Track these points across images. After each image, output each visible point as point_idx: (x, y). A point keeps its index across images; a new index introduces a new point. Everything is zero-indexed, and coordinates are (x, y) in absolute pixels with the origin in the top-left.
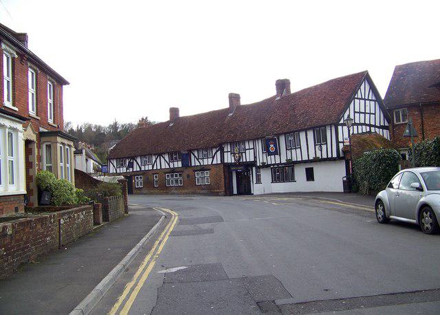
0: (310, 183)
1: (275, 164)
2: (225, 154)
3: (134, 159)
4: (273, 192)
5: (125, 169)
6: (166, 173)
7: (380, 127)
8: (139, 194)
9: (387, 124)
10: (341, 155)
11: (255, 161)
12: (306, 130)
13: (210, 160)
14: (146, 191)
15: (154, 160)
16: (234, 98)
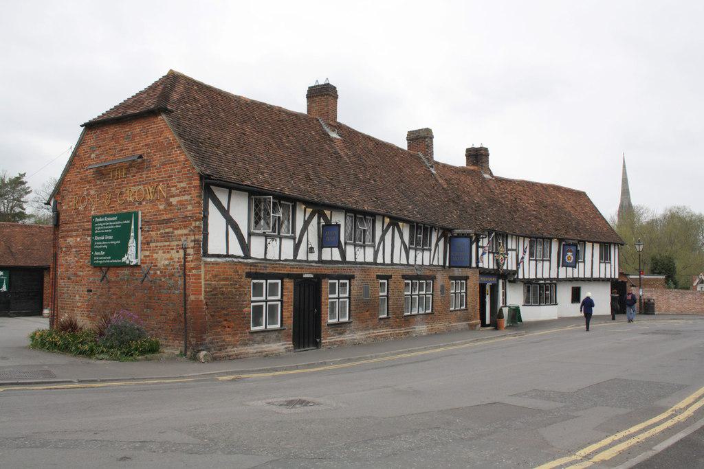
1: (550, 279)
11: (516, 272)
13: (370, 252)
14: (359, 336)
15: (299, 224)
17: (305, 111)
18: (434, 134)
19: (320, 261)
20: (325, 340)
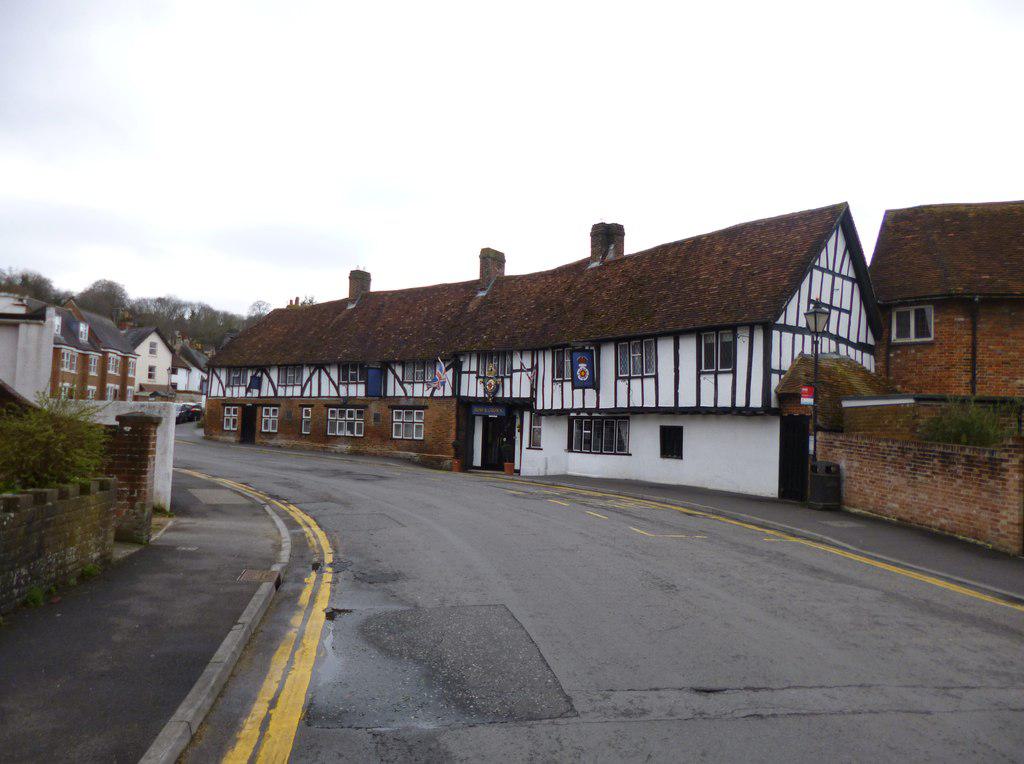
0: (671, 462)
1: (583, 410)
2: (464, 377)
4: (569, 473)
5: (242, 391)
6: (328, 406)
7: (862, 347)
8: (266, 446)
9: (871, 341)
10: (774, 404)
11: (533, 399)
12: (676, 336)
14: (281, 442)
16: (491, 260)
17: (625, 254)
18: (626, 231)
19: (259, 397)
20: (258, 440)
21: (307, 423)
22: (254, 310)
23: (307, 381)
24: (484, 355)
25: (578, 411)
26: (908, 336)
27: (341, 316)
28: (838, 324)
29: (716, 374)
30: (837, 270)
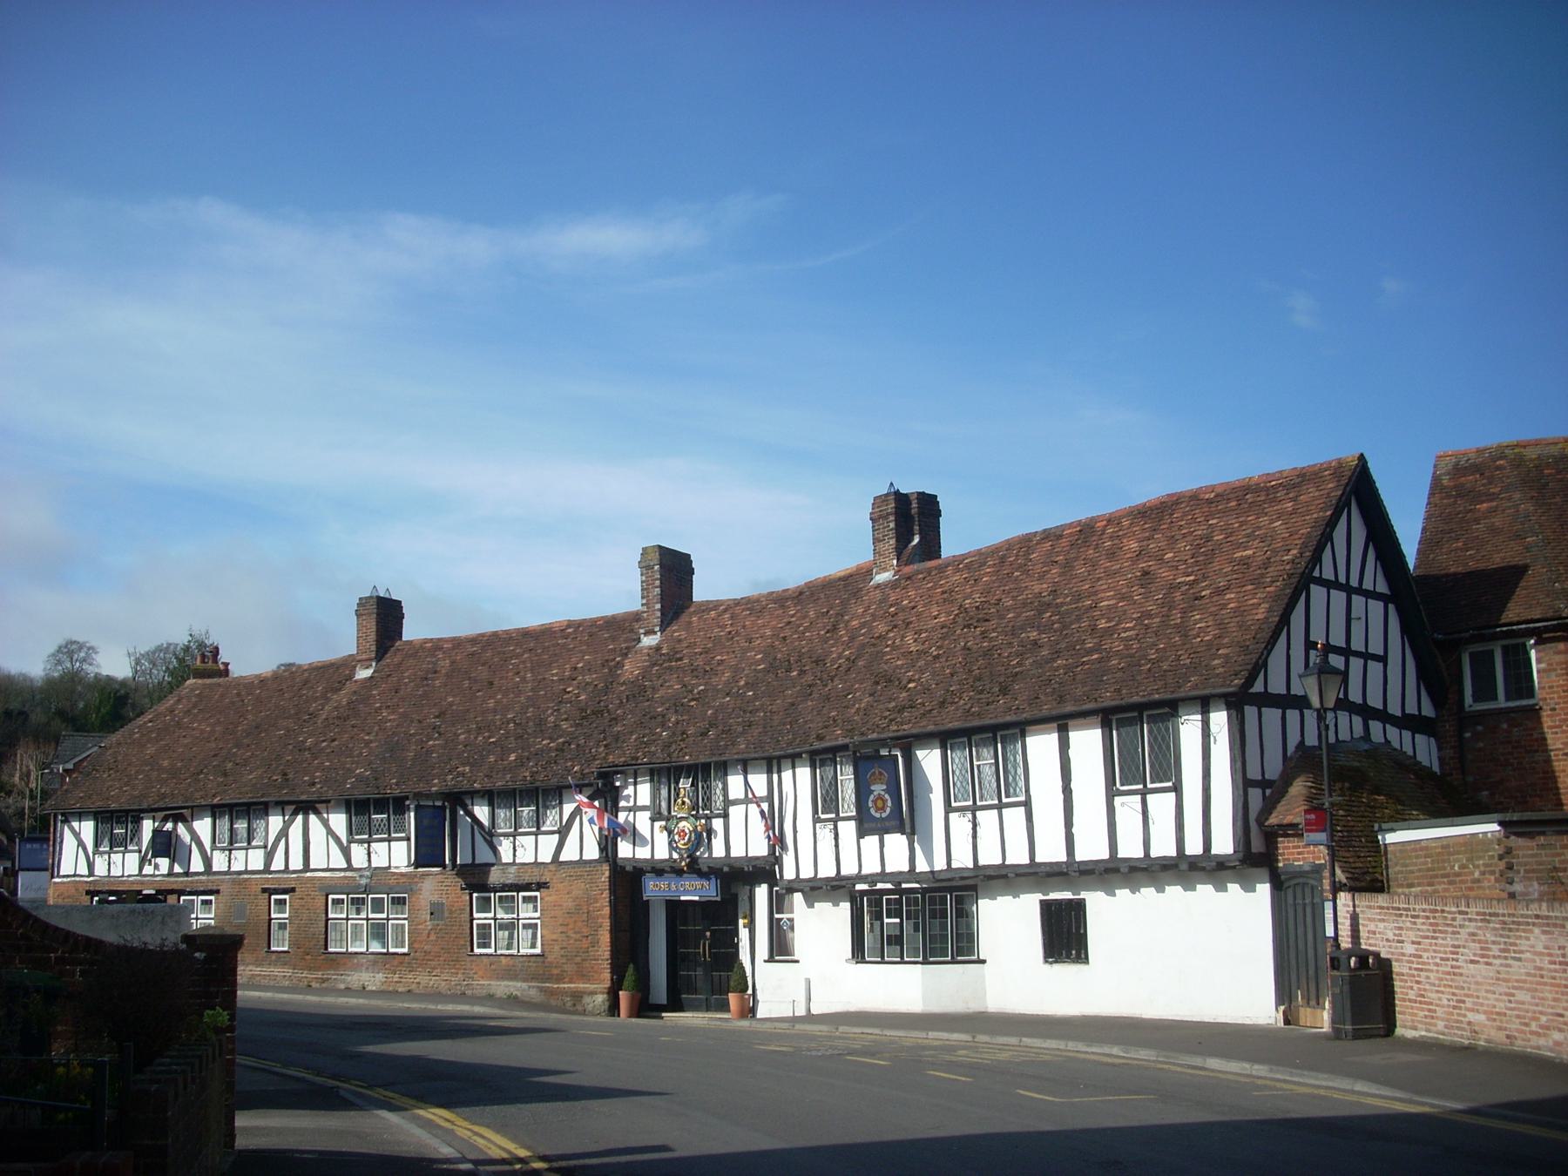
0: (1066, 972)
1: (883, 876)
3: (177, 818)
5: (132, 860)
7: (1409, 723)
9: (1428, 710)
11: (774, 859)
13: (548, 844)
21: (282, 926)
22: (59, 662)
23: (277, 840)
24: (666, 774)
25: (872, 879)
26: (1495, 698)
27: (343, 697)
28: (1368, 685)
29: (1144, 794)
30: (1354, 583)
